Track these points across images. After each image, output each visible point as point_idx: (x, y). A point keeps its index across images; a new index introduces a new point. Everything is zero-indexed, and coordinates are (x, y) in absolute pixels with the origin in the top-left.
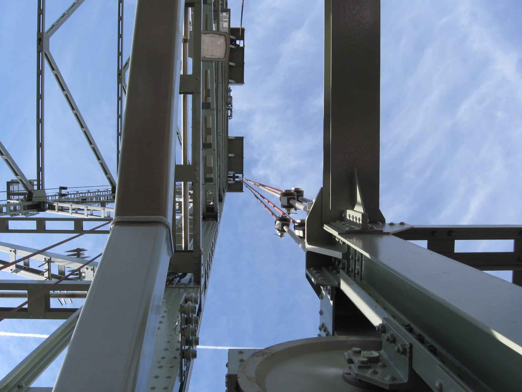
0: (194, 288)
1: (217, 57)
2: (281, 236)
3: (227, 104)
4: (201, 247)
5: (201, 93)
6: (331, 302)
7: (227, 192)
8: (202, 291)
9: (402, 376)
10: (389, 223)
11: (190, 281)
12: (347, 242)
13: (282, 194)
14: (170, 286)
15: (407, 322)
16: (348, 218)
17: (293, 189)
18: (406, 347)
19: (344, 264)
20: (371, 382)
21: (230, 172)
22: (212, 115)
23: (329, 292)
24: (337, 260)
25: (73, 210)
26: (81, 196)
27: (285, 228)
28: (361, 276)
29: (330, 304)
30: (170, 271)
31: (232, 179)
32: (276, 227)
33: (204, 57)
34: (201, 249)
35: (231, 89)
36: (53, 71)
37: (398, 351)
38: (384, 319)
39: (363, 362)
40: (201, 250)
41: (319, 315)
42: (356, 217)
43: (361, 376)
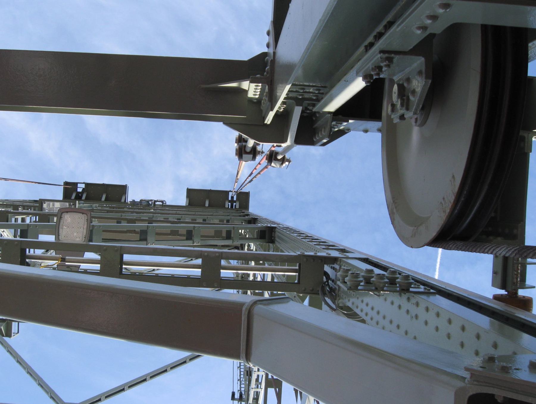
0: (340, 265)
1: (86, 223)
2: (289, 161)
3: (149, 206)
4: (295, 254)
5: (121, 247)
6: (350, 121)
7: (249, 211)
8: (345, 255)
9: (419, 62)
10: (267, 48)
11: (334, 268)
12: (281, 100)
13: (240, 159)
14: (337, 292)
15: (362, 49)
16: (257, 97)
17: (236, 145)
18: (384, 57)
19: (309, 105)
20: (425, 94)
21: (227, 206)
22: (155, 228)
23: (339, 123)
24: (306, 111)
25: (257, 387)
26: (244, 376)
27: (280, 157)
28: (322, 87)
29: (353, 122)
30: (320, 292)
31: (234, 204)
32: (278, 166)
33: (85, 237)
34: (297, 255)
35: (132, 201)
36: (102, 400)
37: (388, 66)
38: (357, 75)
39: (402, 105)
40: (299, 254)
41: (368, 133)
42: (255, 89)
43: (416, 109)
